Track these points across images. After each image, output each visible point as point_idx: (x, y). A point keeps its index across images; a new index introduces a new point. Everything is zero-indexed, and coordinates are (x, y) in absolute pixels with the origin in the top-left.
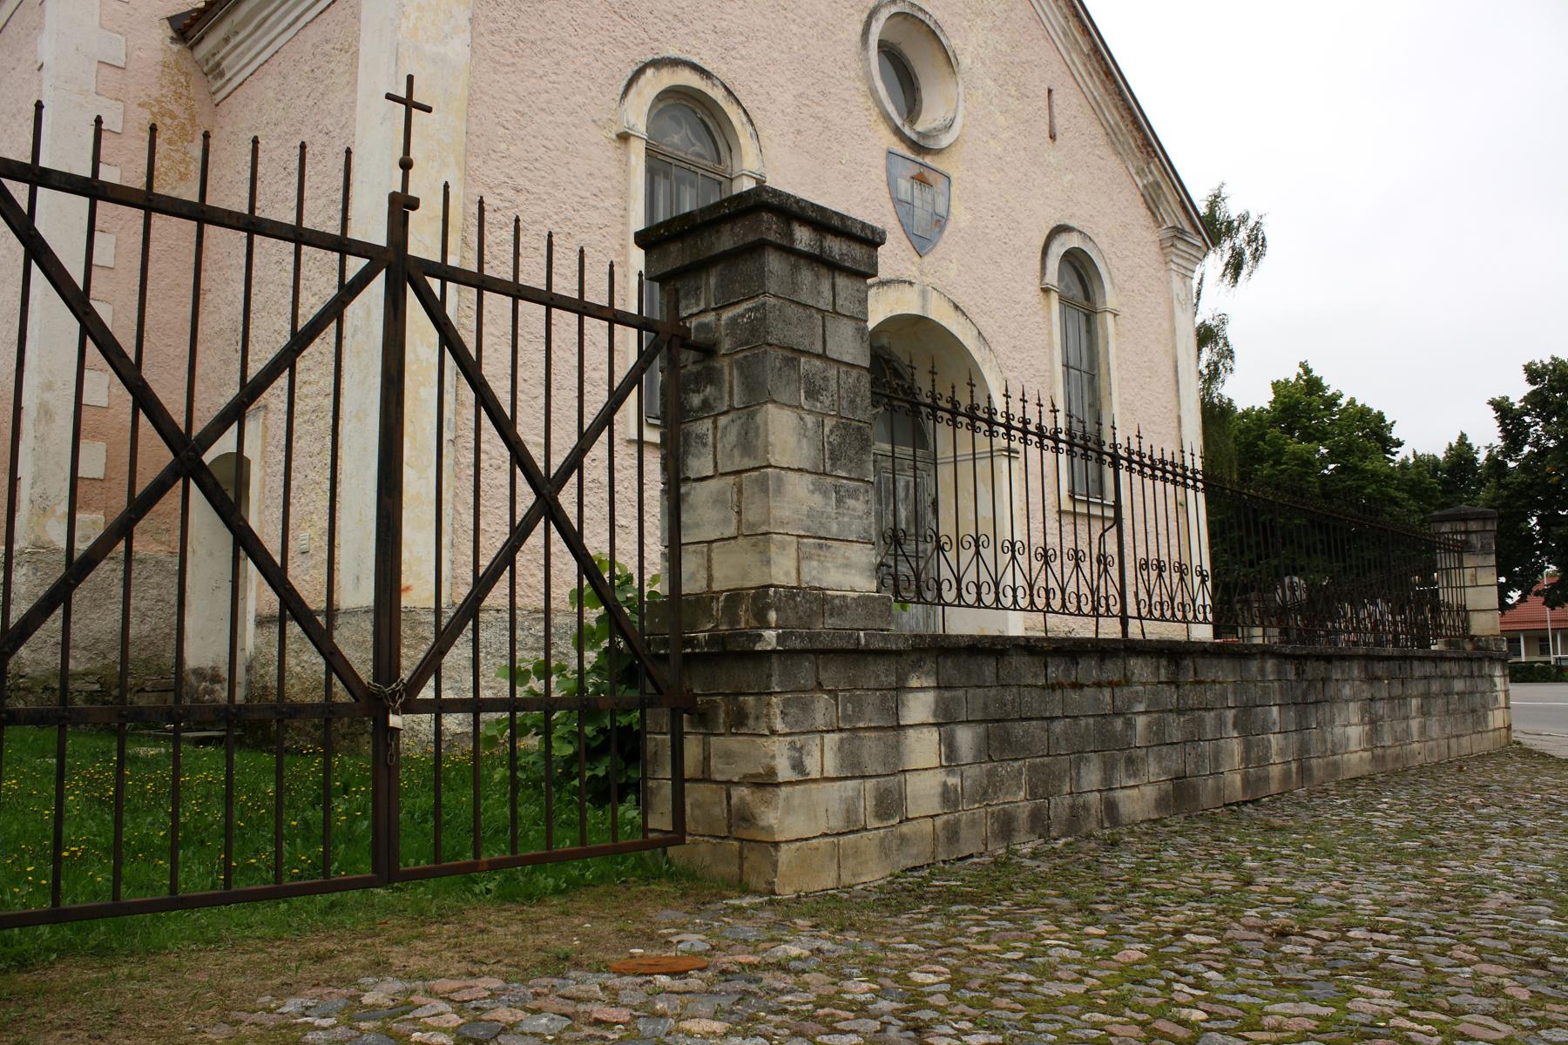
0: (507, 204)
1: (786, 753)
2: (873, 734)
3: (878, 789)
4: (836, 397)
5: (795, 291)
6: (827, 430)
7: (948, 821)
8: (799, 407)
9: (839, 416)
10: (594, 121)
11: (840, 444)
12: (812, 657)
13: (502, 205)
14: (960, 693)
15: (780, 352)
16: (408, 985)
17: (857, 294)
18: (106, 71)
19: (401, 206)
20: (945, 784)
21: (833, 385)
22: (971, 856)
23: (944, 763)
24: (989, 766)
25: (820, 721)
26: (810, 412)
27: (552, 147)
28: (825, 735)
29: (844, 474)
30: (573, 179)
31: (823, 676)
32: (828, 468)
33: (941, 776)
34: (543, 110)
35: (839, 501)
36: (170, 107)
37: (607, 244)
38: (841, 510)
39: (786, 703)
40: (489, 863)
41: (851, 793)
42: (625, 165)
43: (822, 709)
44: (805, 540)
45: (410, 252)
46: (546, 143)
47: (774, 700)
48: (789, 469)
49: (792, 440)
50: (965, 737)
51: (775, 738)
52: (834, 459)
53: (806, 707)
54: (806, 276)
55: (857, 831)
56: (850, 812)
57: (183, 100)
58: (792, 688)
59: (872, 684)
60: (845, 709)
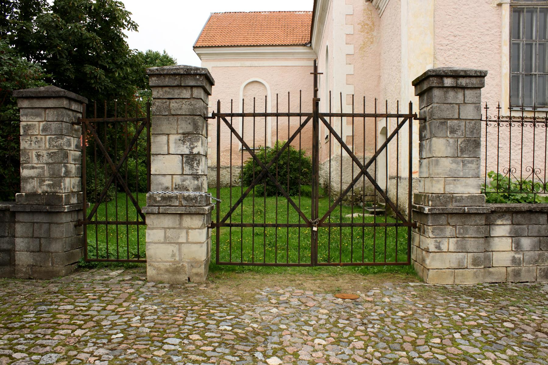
0: (451, 42)
1: (433, 243)
2: (472, 239)
3: (474, 256)
4: (464, 131)
5: (446, 100)
6: (459, 143)
7: (515, 269)
8: (447, 137)
9: (465, 137)
10: (486, 2)
11: (465, 147)
12: (446, 215)
13: (449, 43)
14: (525, 226)
15: (439, 121)
16: (178, 277)
17: (476, 95)
18: (348, 17)
19: (316, 102)
20: (514, 257)
21: (463, 127)
22: (527, 282)
23: (513, 249)
24: (540, 252)
25: (448, 234)
26: (452, 138)
27: (468, 17)
28: (450, 239)
29: (467, 156)
30: (477, 27)
31: (450, 221)
32: (459, 155)
33: (513, 254)
34: (465, 5)
35: (464, 165)
36: (367, 22)
37: (493, 47)
38: (465, 168)
39: (434, 229)
40: (343, 264)
41: (461, 257)
42: (500, 16)
43: (449, 231)
44: (448, 179)
45: (319, 112)
46: (466, 16)
47: (429, 227)
48: (442, 157)
49: (443, 148)
50: (526, 242)
51: (429, 239)
52: (462, 151)
53: (442, 230)
54: (451, 94)
55: (464, 269)
56: (460, 262)
57: (371, 19)
58: (437, 224)
59: (473, 223)
60: (459, 231)
